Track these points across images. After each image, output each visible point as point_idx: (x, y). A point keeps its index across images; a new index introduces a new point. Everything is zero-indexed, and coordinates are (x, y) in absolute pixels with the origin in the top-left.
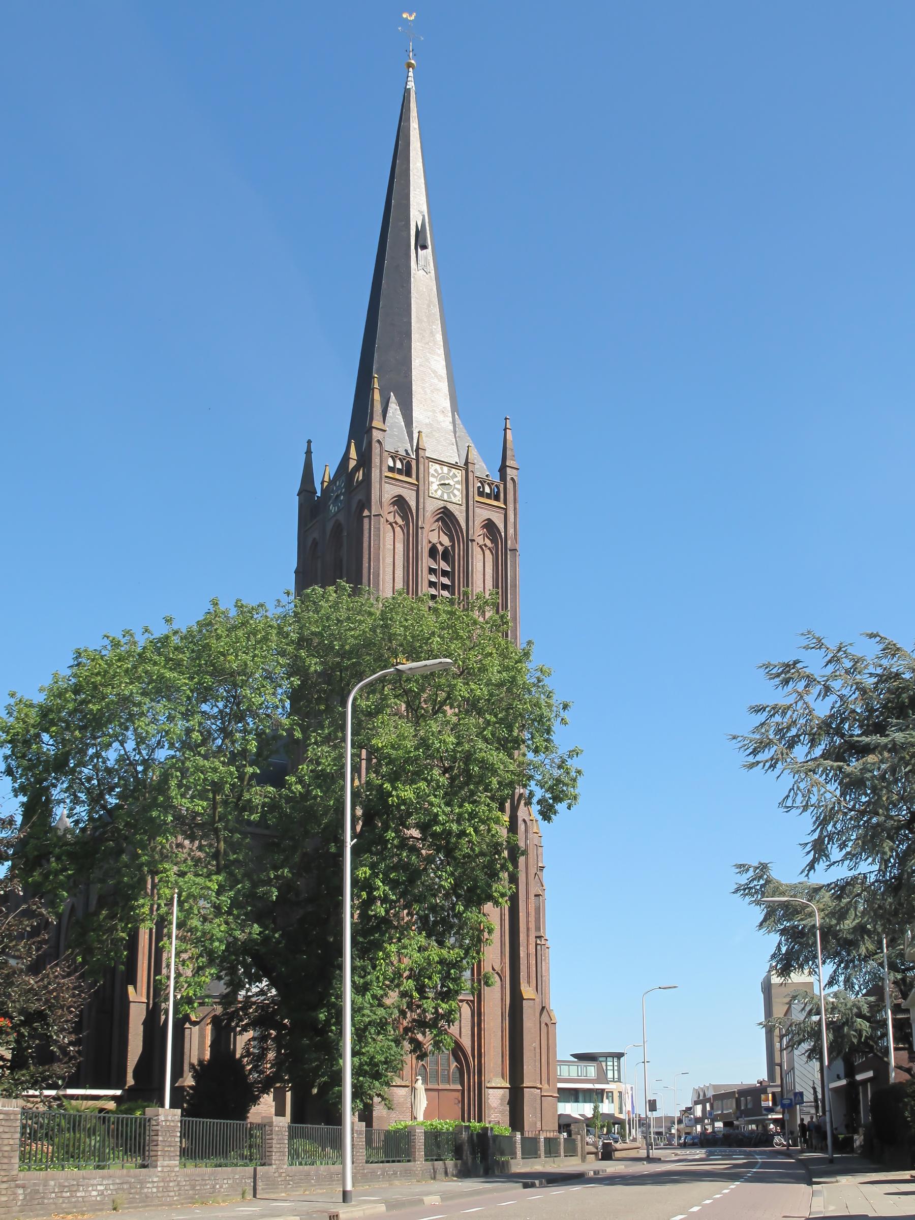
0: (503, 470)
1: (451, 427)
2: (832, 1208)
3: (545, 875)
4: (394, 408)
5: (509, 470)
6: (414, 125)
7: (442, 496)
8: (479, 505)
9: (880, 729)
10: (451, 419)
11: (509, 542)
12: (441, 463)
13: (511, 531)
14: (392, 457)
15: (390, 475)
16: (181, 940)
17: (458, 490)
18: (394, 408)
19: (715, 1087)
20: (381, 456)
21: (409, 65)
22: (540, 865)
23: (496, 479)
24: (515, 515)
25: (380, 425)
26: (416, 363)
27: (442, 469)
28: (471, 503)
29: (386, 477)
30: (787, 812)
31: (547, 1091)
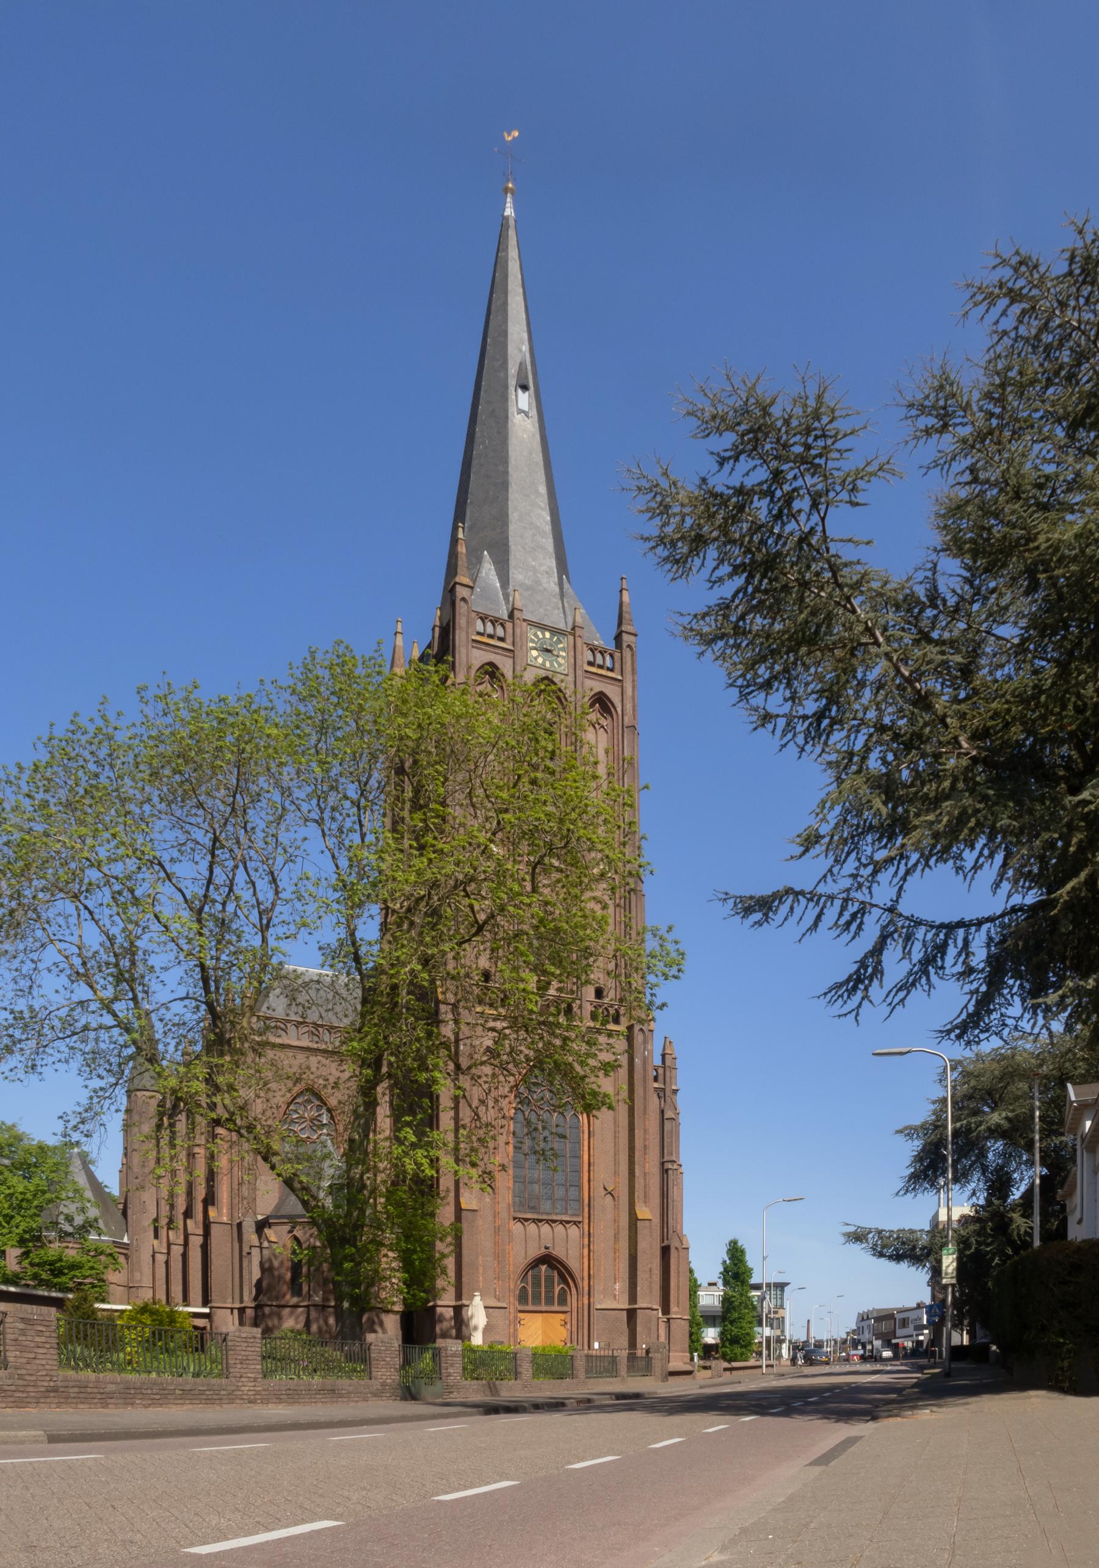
0: (618, 638)
1: (557, 589)
2: (542, 505)
3: (680, 1099)
4: (488, 570)
5: (625, 637)
6: (513, 253)
7: (544, 664)
8: (588, 675)
9: (570, 714)
10: (556, 579)
11: (626, 719)
12: (543, 628)
13: (629, 706)
14: (481, 618)
15: (479, 638)
16: (411, 983)
17: (563, 658)
18: (488, 570)
19: (878, 1310)
20: (468, 617)
21: (506, 190)
22: (674, 1087)
23: (611, 646)
24: (633, 687)
25: (466, 580)
26: (513, 516)
27: (544, 635)
28: (579, 672)
29: (474, 641)
30: (856, 934)
31: (676, 1313)
